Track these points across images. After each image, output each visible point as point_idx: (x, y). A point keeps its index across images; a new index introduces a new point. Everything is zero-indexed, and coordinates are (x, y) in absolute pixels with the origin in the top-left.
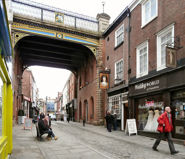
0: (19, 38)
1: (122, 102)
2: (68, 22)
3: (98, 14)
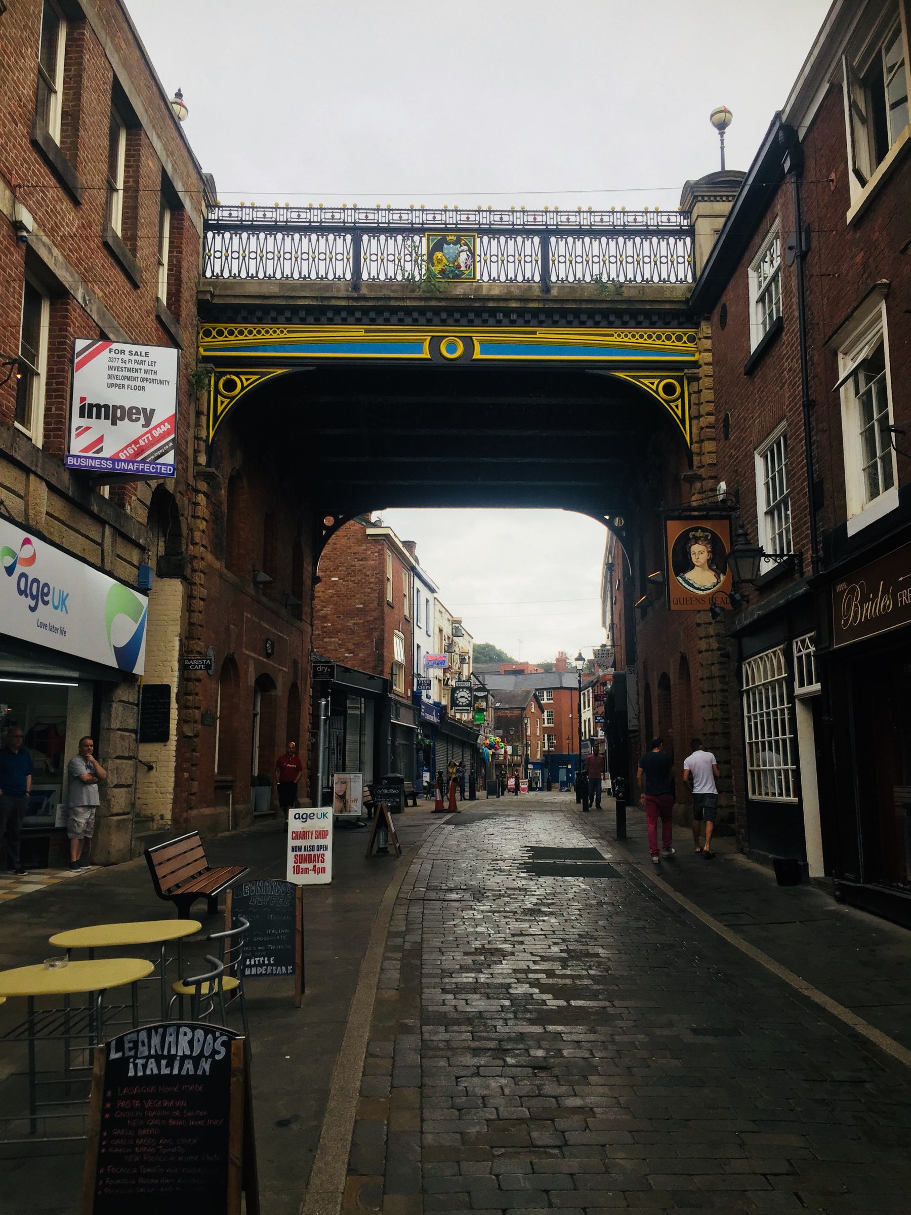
1: (798, 691)
2: (502, 267)
3: (688, 182)
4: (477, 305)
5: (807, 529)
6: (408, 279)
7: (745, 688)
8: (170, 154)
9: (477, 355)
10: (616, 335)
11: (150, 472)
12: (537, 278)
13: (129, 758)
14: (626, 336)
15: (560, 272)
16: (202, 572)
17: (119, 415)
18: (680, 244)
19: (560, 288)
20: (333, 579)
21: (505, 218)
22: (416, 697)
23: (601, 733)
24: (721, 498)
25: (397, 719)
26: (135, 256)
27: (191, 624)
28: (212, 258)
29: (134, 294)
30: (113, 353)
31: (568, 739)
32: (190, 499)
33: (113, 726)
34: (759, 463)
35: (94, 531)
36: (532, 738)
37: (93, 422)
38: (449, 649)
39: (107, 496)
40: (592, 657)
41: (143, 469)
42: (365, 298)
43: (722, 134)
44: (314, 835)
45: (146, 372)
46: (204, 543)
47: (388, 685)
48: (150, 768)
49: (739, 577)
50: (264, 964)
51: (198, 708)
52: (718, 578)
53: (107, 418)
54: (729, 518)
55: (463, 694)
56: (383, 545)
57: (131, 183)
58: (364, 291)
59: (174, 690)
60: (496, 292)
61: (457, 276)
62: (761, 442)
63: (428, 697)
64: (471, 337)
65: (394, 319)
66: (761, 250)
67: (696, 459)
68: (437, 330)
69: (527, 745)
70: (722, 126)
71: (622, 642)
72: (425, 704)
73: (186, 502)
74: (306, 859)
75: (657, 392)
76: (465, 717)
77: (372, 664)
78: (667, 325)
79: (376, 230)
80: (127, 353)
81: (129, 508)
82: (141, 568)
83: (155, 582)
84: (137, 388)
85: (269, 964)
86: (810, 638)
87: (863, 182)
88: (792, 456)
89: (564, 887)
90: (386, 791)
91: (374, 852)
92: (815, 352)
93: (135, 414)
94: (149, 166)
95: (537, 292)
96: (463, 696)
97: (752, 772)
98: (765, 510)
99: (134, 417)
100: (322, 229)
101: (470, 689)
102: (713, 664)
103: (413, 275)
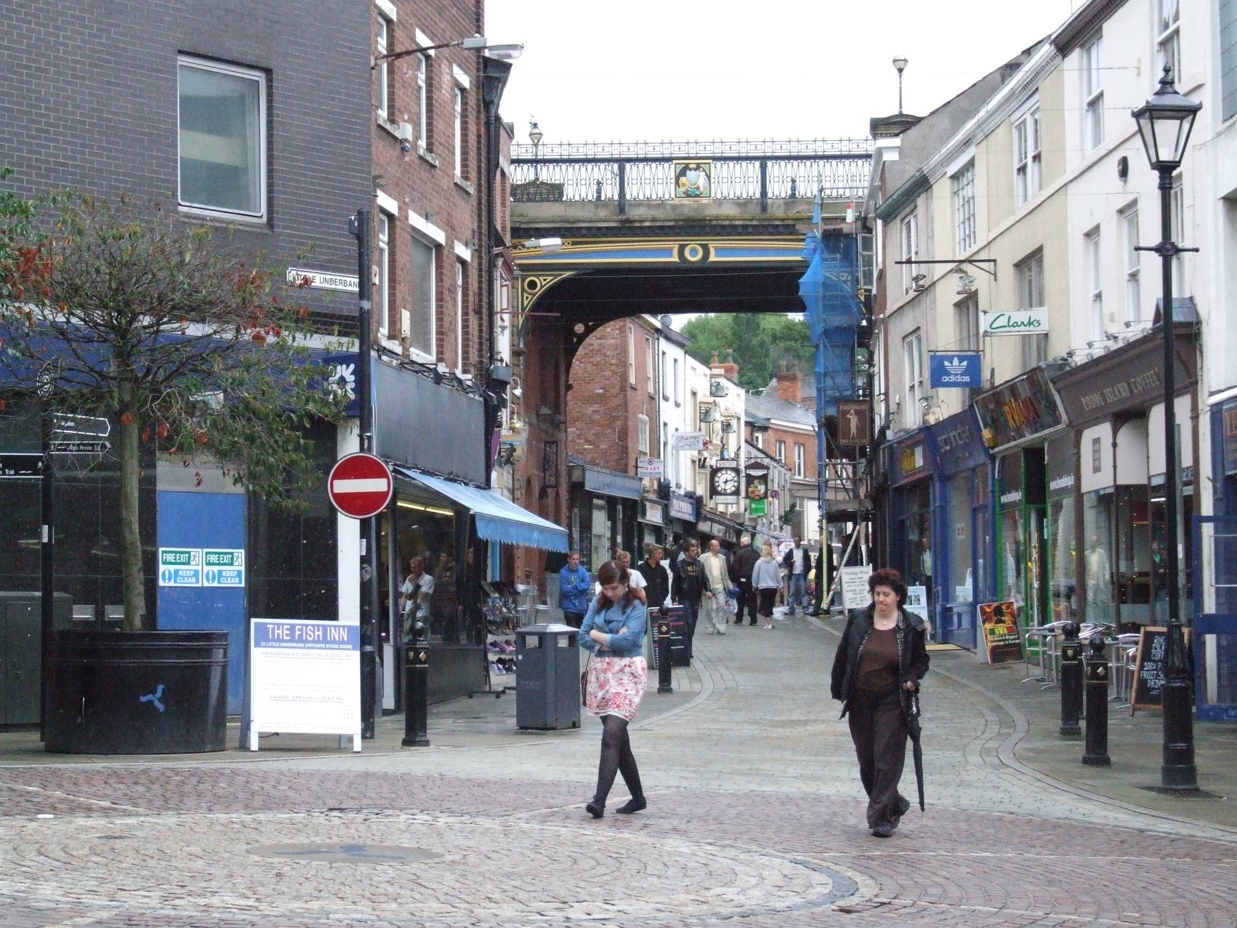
0: (539, 291)
9: (713, 258)
58: (634, 213)
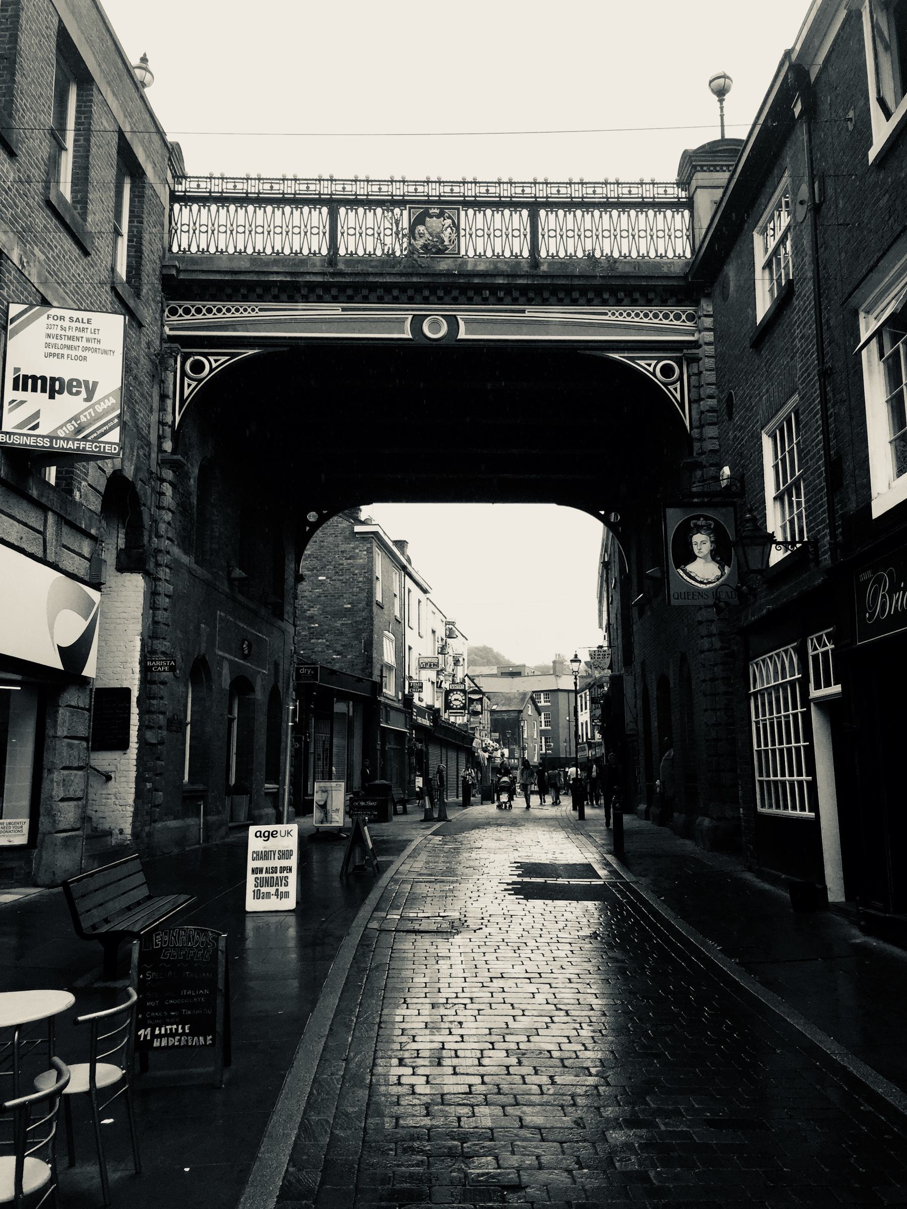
1: (814, 694)
2: (490, 240)
3: (685, 152)
4: (461, 281)
5: (824, 512)
6: (388, 255)
7: (752, 690)
8: (128, 115)
9: (462, 335)
10: (610, 314)
11: (93, 451)
12: (526, 254)
13: (79, 768)
14: (621, 314)
15: (549, 248)
16: (167, 566)
17: (57, 388)
18: (678, 217)
19: (550, 264)
20: (320, 578)
21: (492, 190)
22: (408, 701)
23: (598, 736)
24: (724, 483)
25: (387, 723)
26: (85, 220)
27: (155, 623)
28: (179, 231)
29: (84, 261)
30: (51, 319)
31: (565, 742)
32: (153, 489)
33: (59, 734)
34: (767, 443)
35: (34, 518)
36: (529, 741)
37: (28, 395)
38: (442, 651)
39: (53, 482)
40: (588, 659)
41: (84, 449)
42: (342, 274)
43: (721, 101)
44: (277, 855)
45: (88, 340)
46: (170, 535)
47: (377, 688)
48: (108, 778)
49: (748, 566)
50: (177, 1034)
51: (163, 713)
52: (722, 568)
53: (43, 390)
54: (733, 504)
55: (456, 696)
56: (371, 543)
57: (82, 142)
58: (341, 266)
59: (135, 694)
60: (481, 267)
61: (439, 251)
62: (768, 422)
63: (421, 700)
64: (455, 316)
65: (372, 297)
66: (768, 210)
67: (696, 445)
68: (420, 308)
69: (524, 749)
70: (721, 93)
71: (619, 642)
72: (416, 707)
73: (149, 491)
74: (268, 882)
75: (654, 374)
76: (460, 720)
77: (360, 667)
78: (664, 303)
79: (354, 203)
80: (67, 319)
81: (78, 493)
82: (95, 562)
83: (110, 575)
84: (77, 358)
85: (184, 1033)
86: (827, 634)
87: (888, 115)
88: (806, 432)
89: (554, 914)
90: (363, 804)
91: (350, 870)
92: (831, 314)
93: (75, 387)
94: (101, 122)
95: (526, 268)
96: (457, 699)
97: (761, 782)
98: (774, 495)
99: (74, 390)
100: (296, 201)
101: (464, 691)
102: (715, 665)
103: (393, 250)
